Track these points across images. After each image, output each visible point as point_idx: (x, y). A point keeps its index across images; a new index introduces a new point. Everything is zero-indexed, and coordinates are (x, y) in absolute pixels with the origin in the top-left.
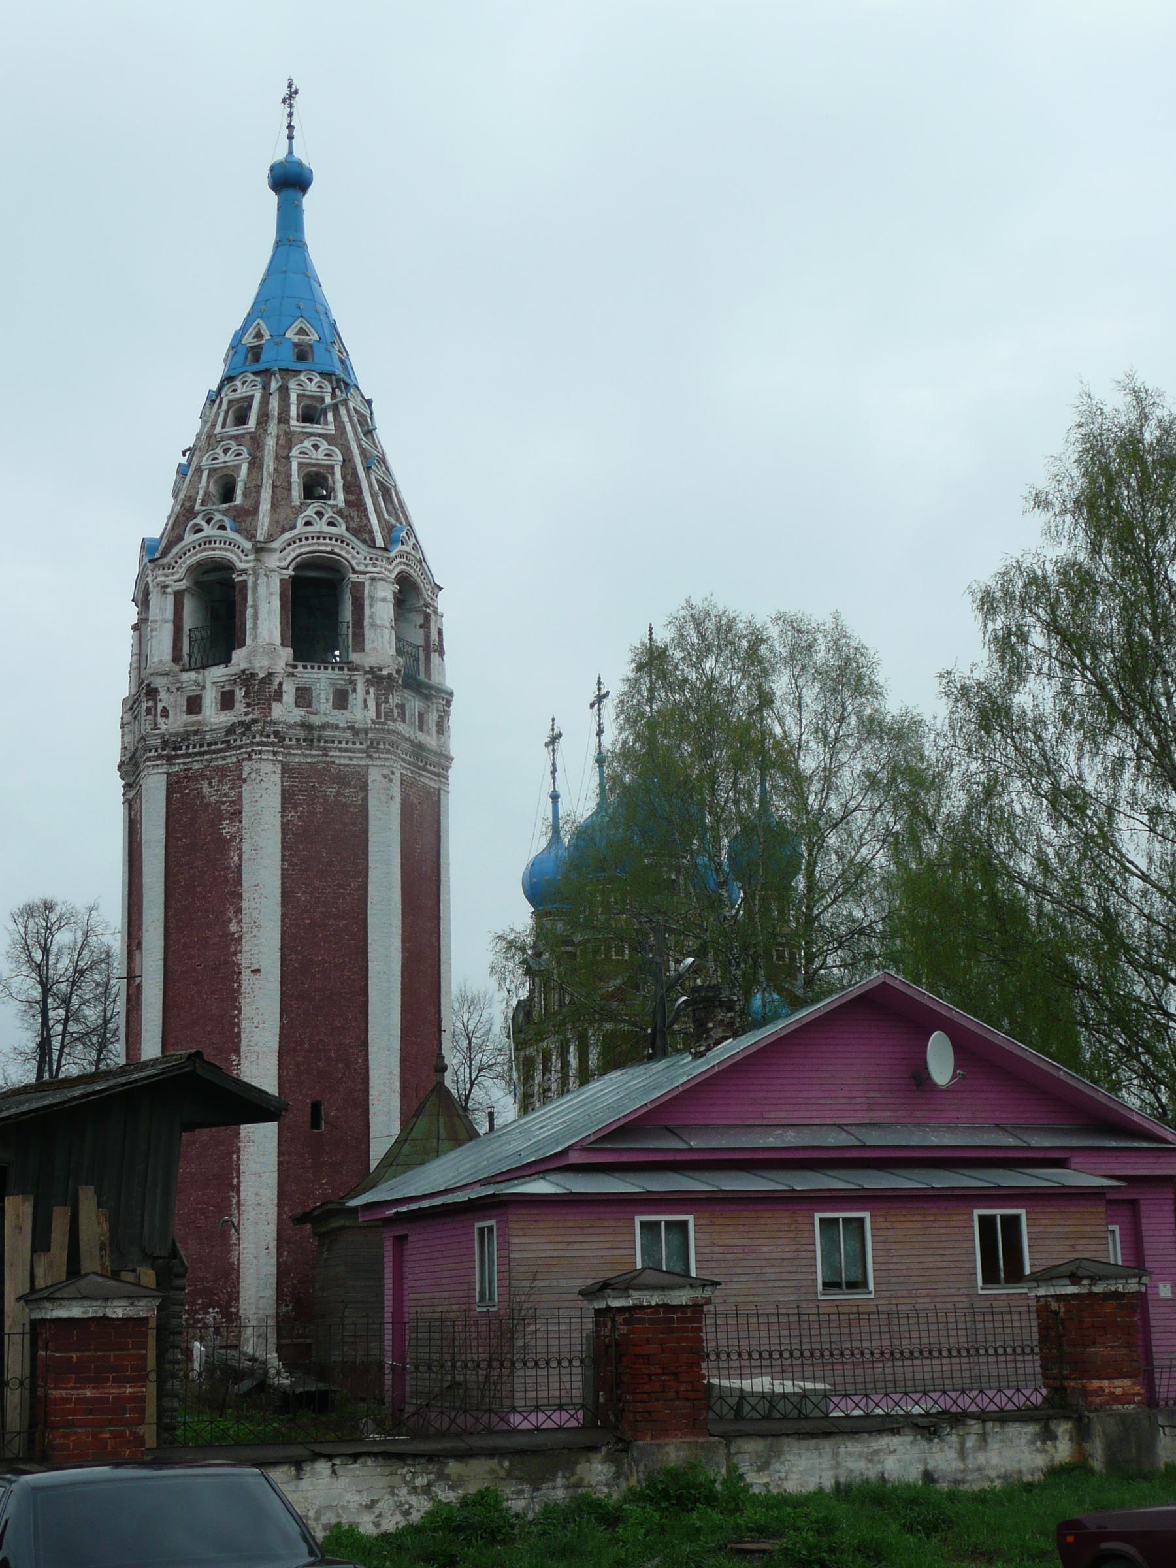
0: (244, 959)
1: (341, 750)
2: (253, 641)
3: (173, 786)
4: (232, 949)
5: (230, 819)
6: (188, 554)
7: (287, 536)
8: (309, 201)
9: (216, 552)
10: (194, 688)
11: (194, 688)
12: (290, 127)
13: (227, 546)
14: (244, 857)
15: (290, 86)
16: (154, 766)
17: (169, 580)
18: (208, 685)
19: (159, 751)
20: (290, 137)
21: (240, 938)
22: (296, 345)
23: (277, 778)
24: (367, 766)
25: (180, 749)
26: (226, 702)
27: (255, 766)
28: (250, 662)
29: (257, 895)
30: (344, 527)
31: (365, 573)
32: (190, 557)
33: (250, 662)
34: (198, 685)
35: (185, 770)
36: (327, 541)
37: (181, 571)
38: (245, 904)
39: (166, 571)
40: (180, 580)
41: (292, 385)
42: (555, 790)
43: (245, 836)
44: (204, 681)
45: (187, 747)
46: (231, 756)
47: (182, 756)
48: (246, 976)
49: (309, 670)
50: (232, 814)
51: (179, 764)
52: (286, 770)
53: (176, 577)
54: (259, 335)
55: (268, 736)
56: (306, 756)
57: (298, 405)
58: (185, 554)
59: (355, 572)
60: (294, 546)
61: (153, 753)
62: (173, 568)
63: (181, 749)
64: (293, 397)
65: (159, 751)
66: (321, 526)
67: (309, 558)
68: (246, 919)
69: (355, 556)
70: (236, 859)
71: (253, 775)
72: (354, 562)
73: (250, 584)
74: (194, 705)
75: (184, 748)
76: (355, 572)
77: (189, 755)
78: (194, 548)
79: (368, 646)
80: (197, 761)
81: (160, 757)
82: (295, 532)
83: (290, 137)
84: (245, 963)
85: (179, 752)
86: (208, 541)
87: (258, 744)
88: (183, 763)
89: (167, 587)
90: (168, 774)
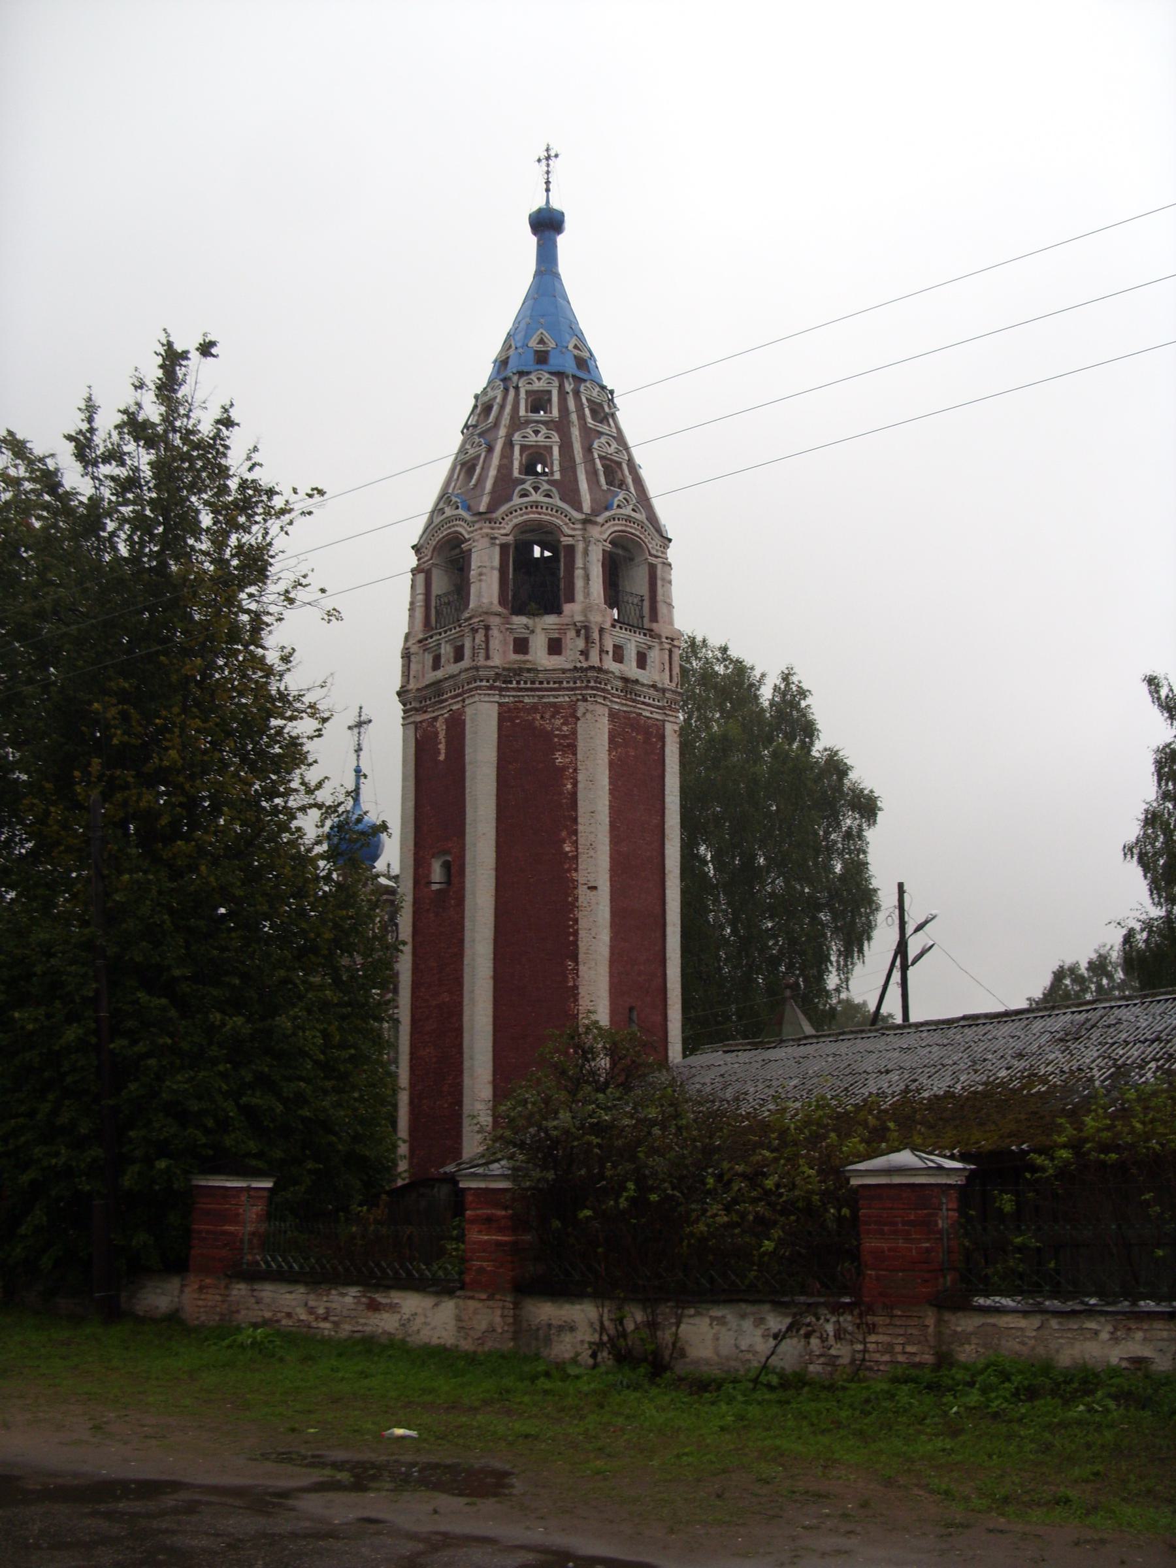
0: (581, 877)
1: (644, 703)
2: (585, 598)
3: (507, 718)
4: (566, 866)
5: (562, 751)
6: (514, 514)
7: (607, 514)
8: (561, 240)
9: (542, 516)
10: (523, 631)
11: (523, 631)
12: (548, 183)
13: (554, 512)
14: (580, 786)
15: (547, 150)
16: (485, 694)
17: (496, 533)
18: (538, 630)
19: (491, 681)
20: (548, 190)
21: (576, 857)
22: (537, 352)
23: (605, 720)
24: (664, 721)
25: (511, 682)
26: (555, 647)
27: (590, 707)
28: (586, 616)
29: (592, 821)
30: (644, 516)
31: (657, 557)
32: (516, 517)
33: (586, 616)
34: (528, 628)
35: (516, 702)
36: (636, 526)
37: (507, 528)
38: (580, 828)
39: (492, 525)
40: (506, 535)
41: (582, 389)
42: (358, 766)
43: (580, 767)
44: (535, 627)
45: (518, 683)
46: (563, 695)
47: (513, 688)
48: (582, 891)
49: (618, 629)
50: (565, 746)
51: (509, 696)
52: (613, 715)
53: (503, 531)
54: (541, 341)
55: (600, 683)
56: (623, 705)
57: (526, 400)
58: (511, 513)
59: (651, 555)
60: (612, 522)
61: (484, 683)
62: (500, 523)
63: (511, 683)
64: (523, 395)
65: (491, 681)
66: (535, 497)
67: (620, 536)
68: (581, 841)
69: (570, 533)
70: (569, 786)
71: (589, 716)
72: (650, 546)
73: (580, 547)
74: (521, 646)
75: (514, 682)
76: (651, 555)
77: (520, 690)
78: (526, 508)
79: (660, 618)
80: (528, 696)
81: (491, 688)
82: (512, 503)
83: (548, 190)
84: (581, 880)
85: (510, 686)
86: (536, 504)
87: (592, 688)
88: (513, 696)
89: (495, 538)
90: (500, 704)
